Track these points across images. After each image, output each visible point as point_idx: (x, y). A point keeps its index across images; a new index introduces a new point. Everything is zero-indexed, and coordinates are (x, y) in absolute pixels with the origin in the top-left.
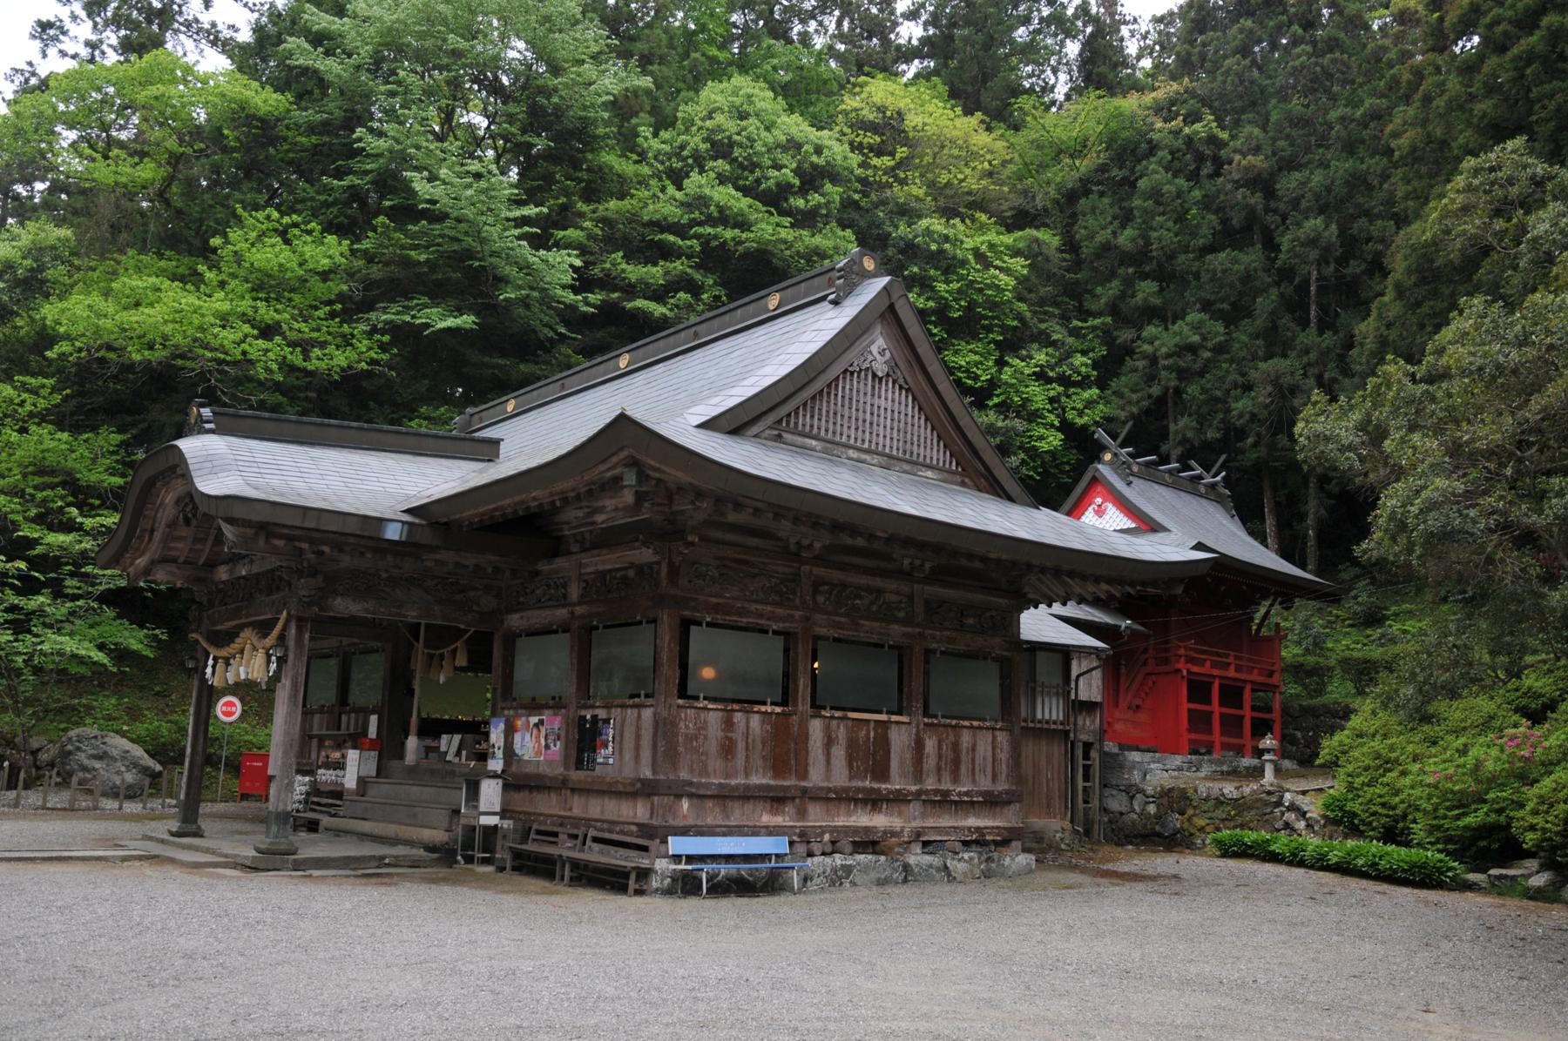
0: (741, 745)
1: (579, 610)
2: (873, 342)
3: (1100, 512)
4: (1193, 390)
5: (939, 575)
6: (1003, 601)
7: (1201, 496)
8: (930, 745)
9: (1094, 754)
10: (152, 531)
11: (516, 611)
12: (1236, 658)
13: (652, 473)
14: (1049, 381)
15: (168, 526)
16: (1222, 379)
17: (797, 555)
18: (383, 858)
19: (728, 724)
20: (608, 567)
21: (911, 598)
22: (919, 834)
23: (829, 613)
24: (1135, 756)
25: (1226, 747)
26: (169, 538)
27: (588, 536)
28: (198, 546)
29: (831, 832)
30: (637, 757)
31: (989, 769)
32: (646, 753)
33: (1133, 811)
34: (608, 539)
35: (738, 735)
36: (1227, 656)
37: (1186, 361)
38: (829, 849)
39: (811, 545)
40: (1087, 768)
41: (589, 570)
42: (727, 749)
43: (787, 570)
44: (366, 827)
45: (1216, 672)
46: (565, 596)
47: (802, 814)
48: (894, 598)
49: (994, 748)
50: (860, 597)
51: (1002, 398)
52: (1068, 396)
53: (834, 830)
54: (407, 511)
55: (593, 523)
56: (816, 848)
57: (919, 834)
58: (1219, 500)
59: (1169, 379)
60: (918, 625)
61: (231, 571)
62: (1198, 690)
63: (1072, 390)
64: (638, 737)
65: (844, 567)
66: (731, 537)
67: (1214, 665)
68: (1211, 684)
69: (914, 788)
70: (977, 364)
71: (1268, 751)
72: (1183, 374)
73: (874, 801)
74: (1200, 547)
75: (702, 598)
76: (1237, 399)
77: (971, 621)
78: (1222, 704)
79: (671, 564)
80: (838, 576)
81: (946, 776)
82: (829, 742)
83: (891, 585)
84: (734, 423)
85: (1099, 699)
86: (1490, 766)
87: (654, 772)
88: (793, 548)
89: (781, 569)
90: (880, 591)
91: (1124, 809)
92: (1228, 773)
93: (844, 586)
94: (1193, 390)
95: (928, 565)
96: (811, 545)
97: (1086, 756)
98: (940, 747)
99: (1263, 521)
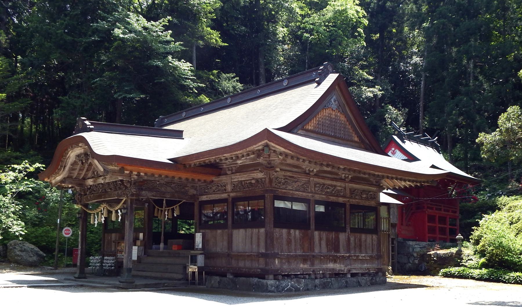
0: (293, 241)
1: (232, 195)
2: (332, 98)
5: (353, 180)
6: (374, 189)
8: (352, 239)
9: (395, 242)
10: (65, 166)
11: (205, 195)
13: (272, 148)
15: (71, 165)
17: (309, 174)
18: (164, 283)
19: (289, 234)
20: (243, 179)
21: (345, 188)
22: (349, 271)
23: (320, 194)
24: (411, 243)
25: (440, 239)
26: (72, 169)
27: (234, 168)
28: (81, 172)
29: (322, 270)
30: (258, 245)
31: (371, 249)
32: (262, 244)
33: (410, 263)
34: (242, 169)
35: (292, 237)
38: (322, 276)
39: (313, 171)
40: (393, 247)
41: (235, 180)
42: (289, 242)
43: (306, 180)
44: (144, 274)
46: (225, 190)
47: (313, 264)
48: (339, 188)
49: (372, 240)
50: (328, 188)
53: (323, 270)
54: (169, 160)
55: (236, 164)
56: (318, 276)
57: (349, 271)
60: (347, 198)
61: (94, 181)
64: (259, 239)
65: (323, 178)
66: (287, 168)
69: (348, 255)
73: (335, 260)
74: (433, 167)
75: (280, 190)
77: (364, 196)
79: (270, 178)
80: (321, 181)
81: (357, 250)
82: (320, 239)
83: (339, 184)
84: (289, 128)
87: (266, 249)
88: (307, 172)
89: (304, 179)
90: (335, 186)
91: (406, 262)
93: (324, 184)
95: (350, 176)
96: (313, 171)
97: (393, 243)
98: (355, 240)
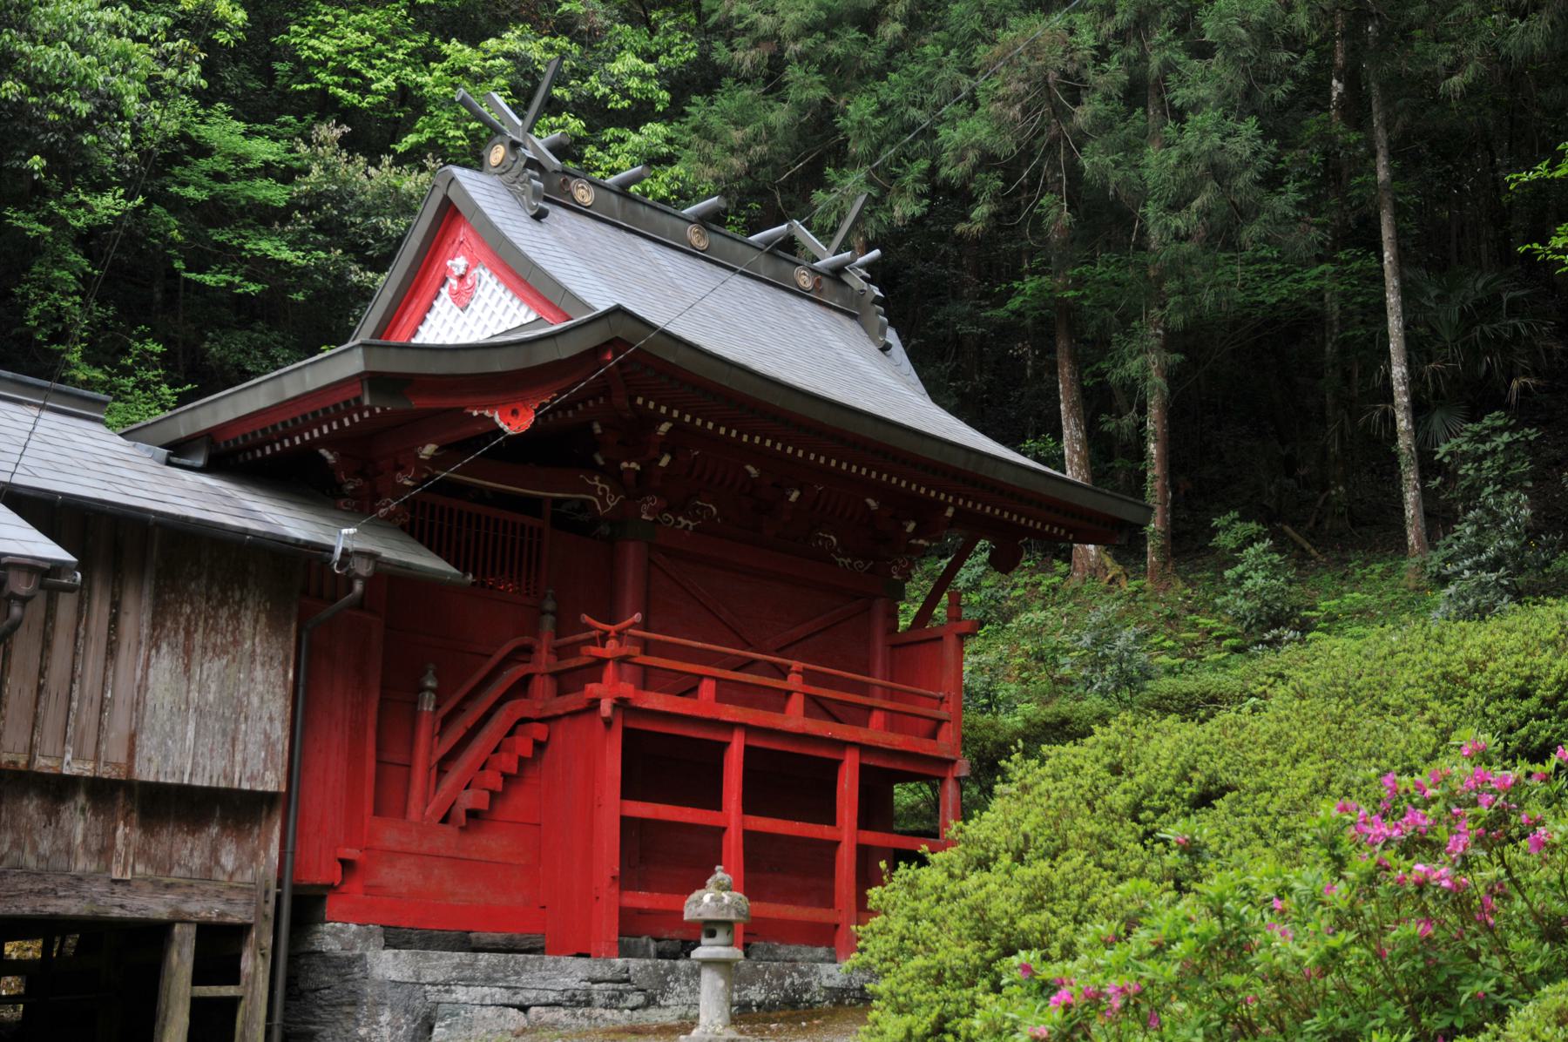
3: (463, 299)
4: (859, 109)
7: (800, 294)
12: (808, 677)
14: (553, 107)
16: (925, 84)
36: (782, 672)
37: (845, 43)
45: (730, 713)
51: (427, 134)
52: (604, 147)
58: (851, 310)
59: (806, 86)
62: (666, 763)
63: (611, 132)
67: (727, 692)
68: (833, 767)
70: (366, 55)
71: (710, 928)
72: (841, 74)
76: (953, 122)
78: (750, 805)
85: (272, 782)
86: (1287, 945)
92: (766, 1008)
94: (859, 109)
99: (1058, 435)
